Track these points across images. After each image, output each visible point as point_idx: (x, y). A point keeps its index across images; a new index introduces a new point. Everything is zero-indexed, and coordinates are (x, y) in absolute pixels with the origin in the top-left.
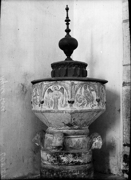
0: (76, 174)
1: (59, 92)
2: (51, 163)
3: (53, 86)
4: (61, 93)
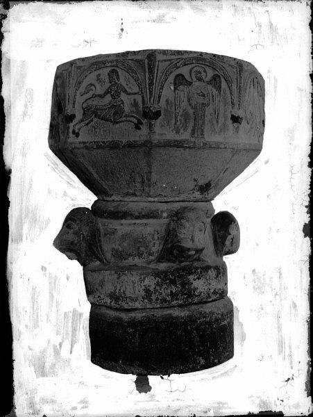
0: (176, 313)
1: (210, 87)
2: (161, 303)
3: (193, 65)
4: (214, 90)
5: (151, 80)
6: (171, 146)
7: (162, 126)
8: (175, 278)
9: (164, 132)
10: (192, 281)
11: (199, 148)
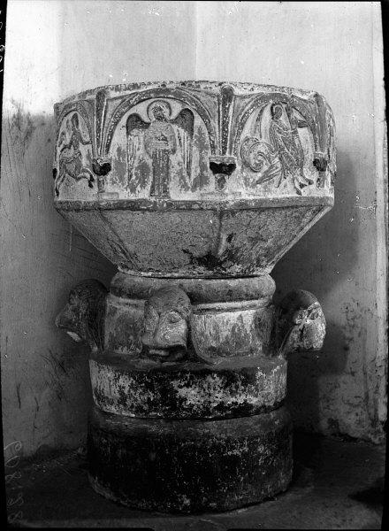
0: (236, 452)
1: (175, 127)
3: (149, 102)
4: (182, 131)
5: (99, 126)
6: (124, 209)
7: (114, 183)
8: (152, 382)
9: (117, 190)
10: (176, 388)
11: (163, 211)
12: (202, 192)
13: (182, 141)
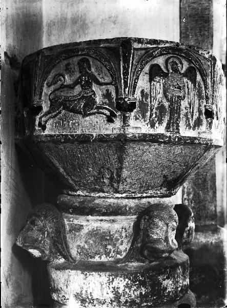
1: (185, 80)
3: (169, 56)
4: (190, 83)
6: (145, 141)
12: (199, 131)
13: (190, 91)
